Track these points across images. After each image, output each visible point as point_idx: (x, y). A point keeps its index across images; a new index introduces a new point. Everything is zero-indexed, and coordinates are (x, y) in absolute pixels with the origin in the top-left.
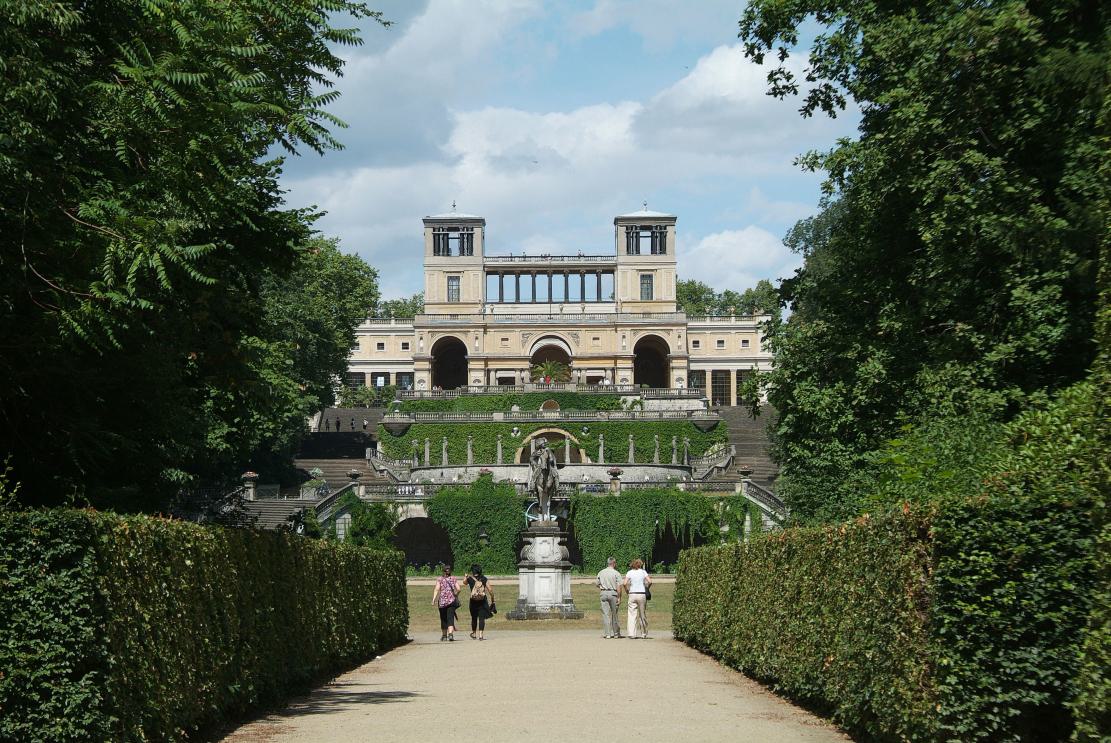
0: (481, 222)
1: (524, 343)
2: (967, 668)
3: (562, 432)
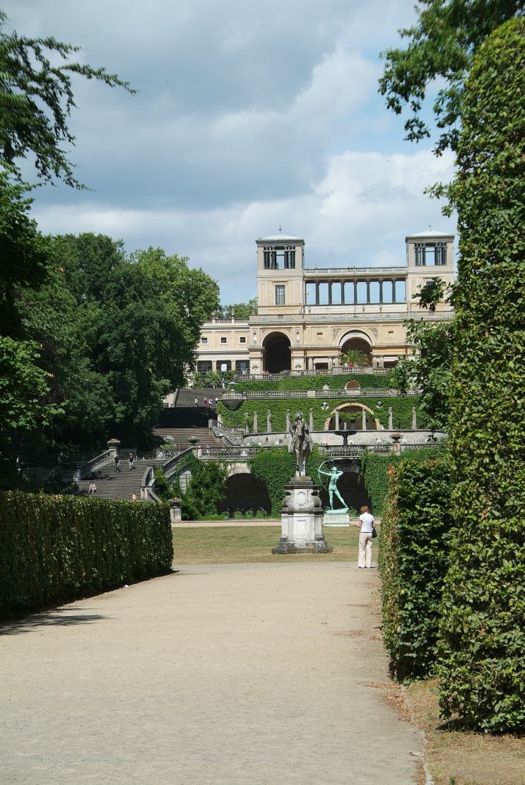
0: (301, 242)
1: (335, 336)
2: (421, 597)
3: (361, 405)
